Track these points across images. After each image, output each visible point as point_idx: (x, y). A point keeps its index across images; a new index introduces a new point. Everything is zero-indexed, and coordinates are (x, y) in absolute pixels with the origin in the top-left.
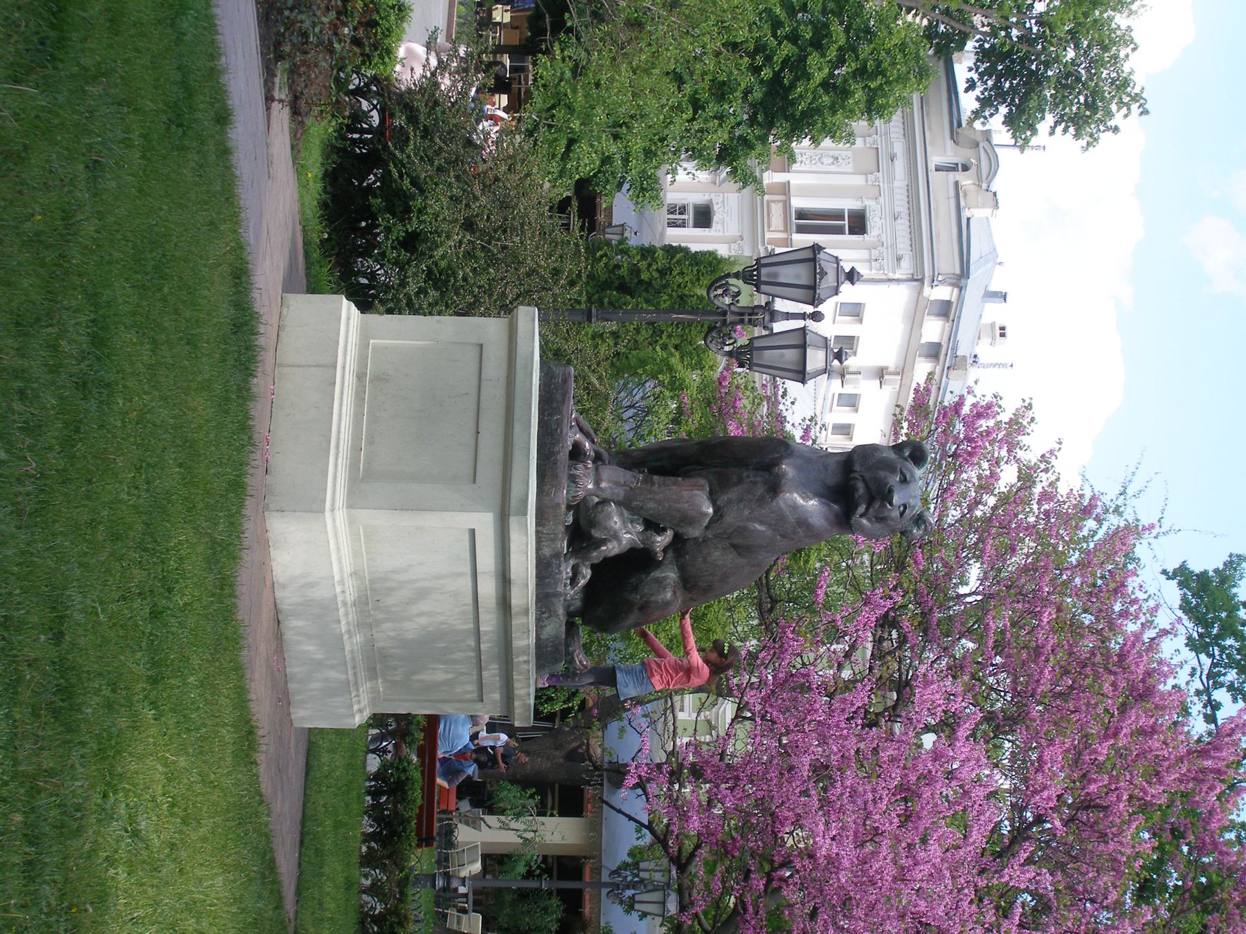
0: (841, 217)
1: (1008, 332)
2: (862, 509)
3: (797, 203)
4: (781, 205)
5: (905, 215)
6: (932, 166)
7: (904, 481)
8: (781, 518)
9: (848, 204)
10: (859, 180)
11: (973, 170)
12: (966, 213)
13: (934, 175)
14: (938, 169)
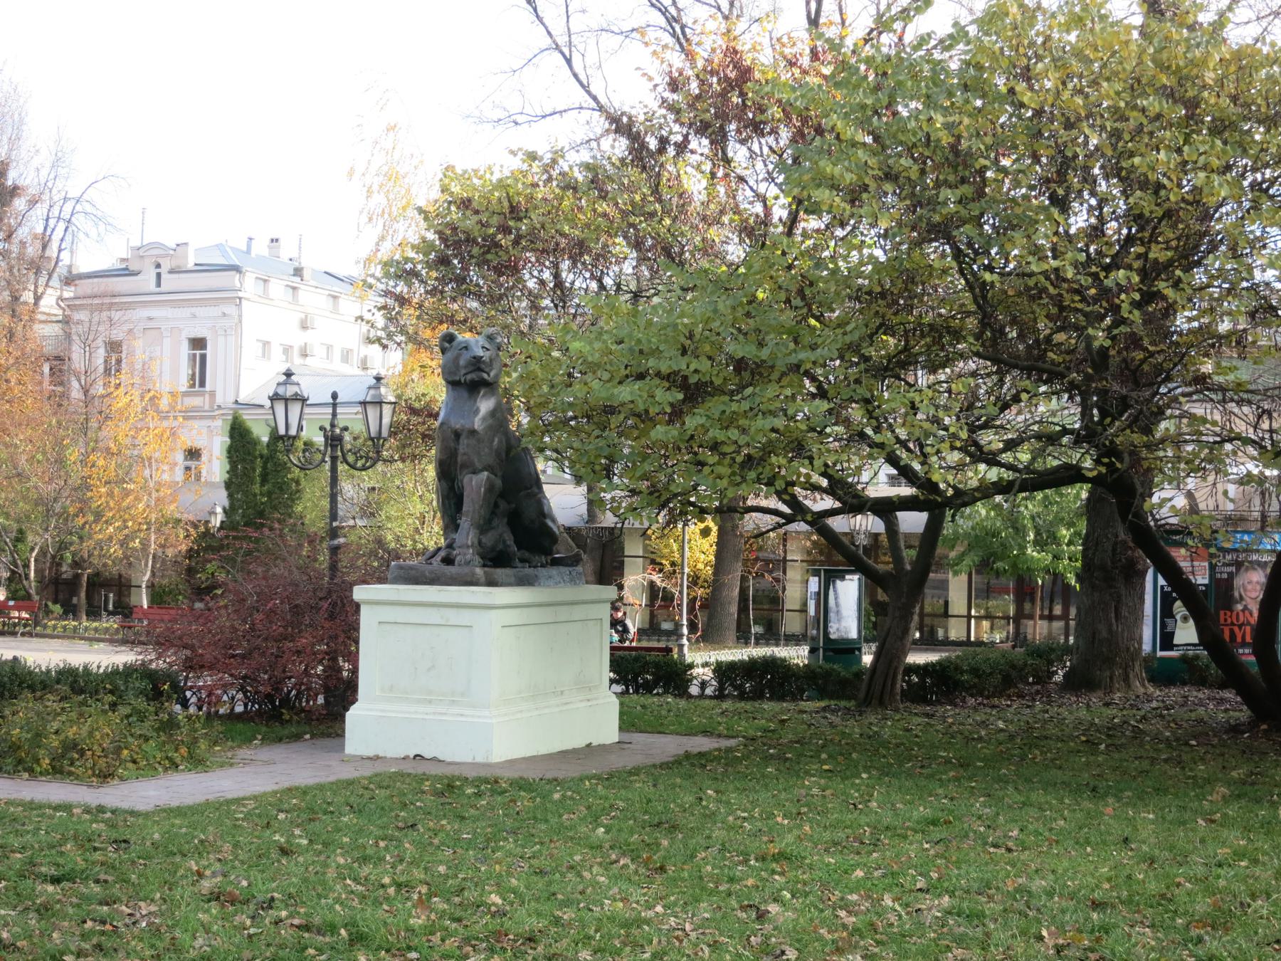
0: (195, 355)
1: (275, 237)
2: (485, 376)
3: (183, 385)
4: (186, 399)
5: (194, 310)
6: (158, 290)
7: (466, 348)
8: (490, 427)
9: (185, 350)
10: (167, 342)
11: (161, 261)
12: (190, 266)
13: (164, 288)
14: (159, 284)
